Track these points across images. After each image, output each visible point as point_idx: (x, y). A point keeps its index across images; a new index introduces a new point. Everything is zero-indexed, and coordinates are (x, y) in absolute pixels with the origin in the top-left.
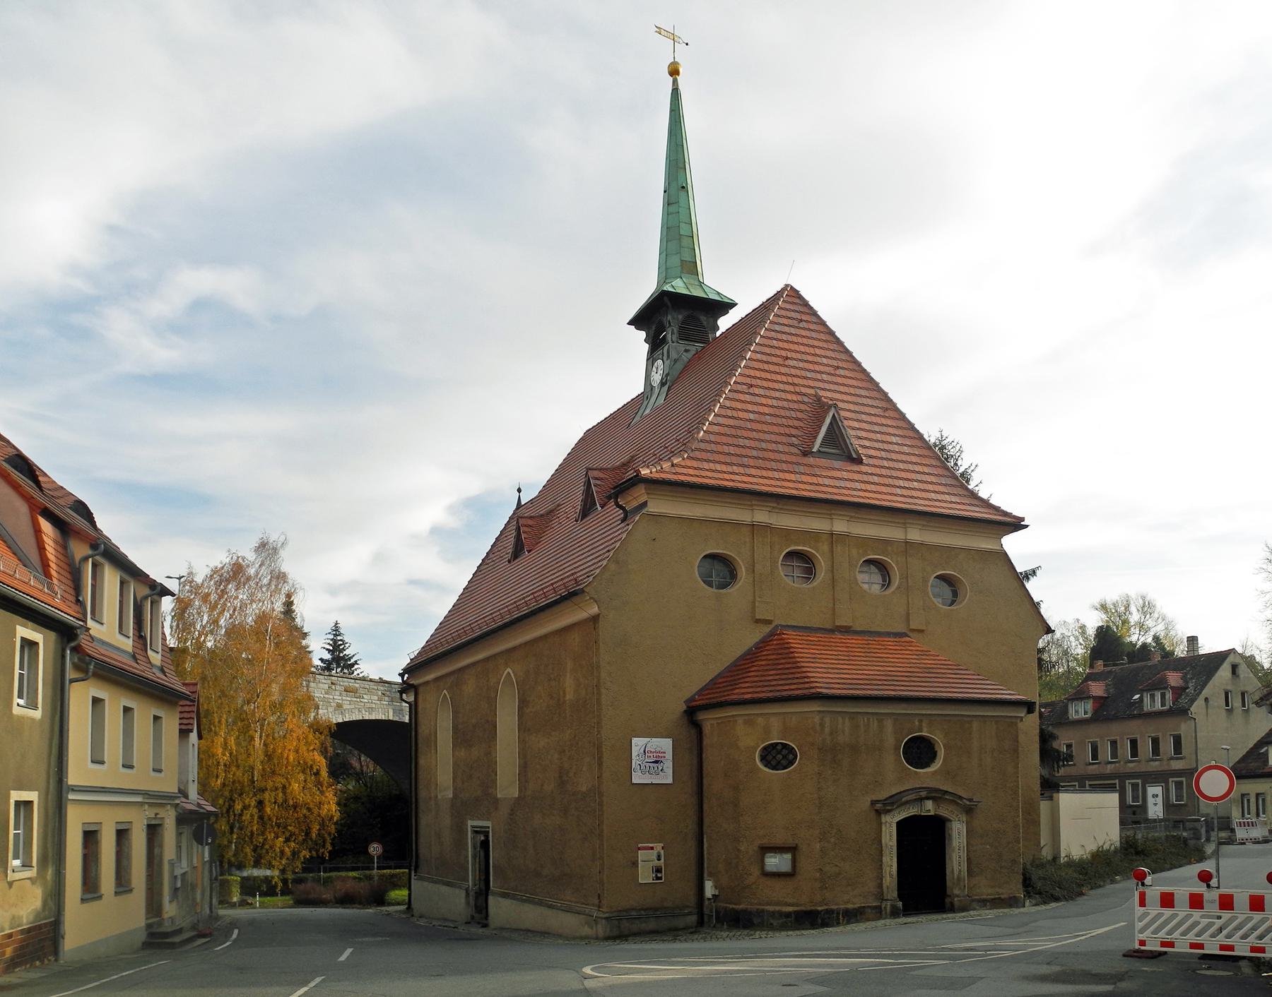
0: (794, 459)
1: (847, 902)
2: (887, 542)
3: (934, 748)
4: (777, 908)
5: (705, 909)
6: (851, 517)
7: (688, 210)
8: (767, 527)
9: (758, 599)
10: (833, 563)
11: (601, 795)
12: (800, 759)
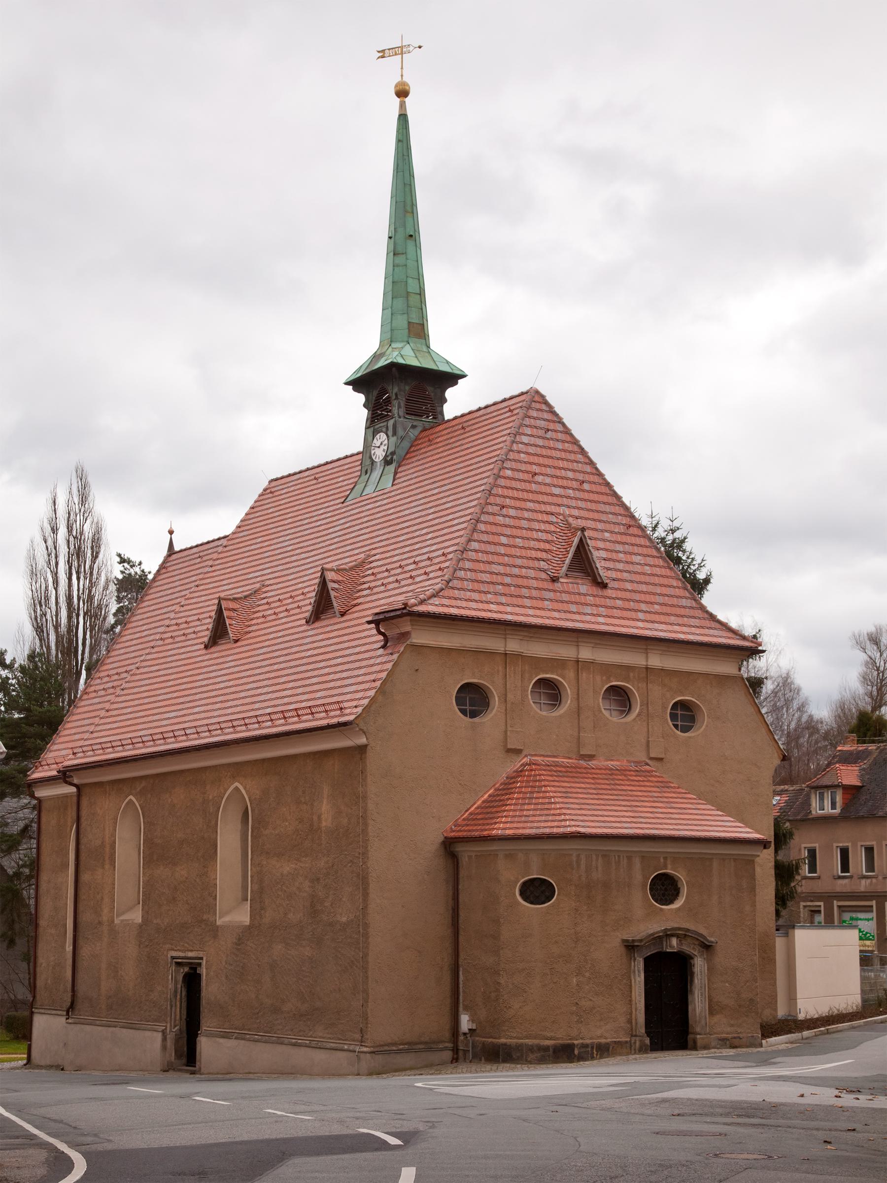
0: (541, 584)
1: (601, 1037)
2: (629, 668)
3: (677, 885)
4: (536, 1042)
5: (460, 1044)
6: (596, 644)
7: (416, 264)
8: (519, 656)
9: (509, 729)
10: (578, 689)
11: (366, 926)
12: (558, 895)
